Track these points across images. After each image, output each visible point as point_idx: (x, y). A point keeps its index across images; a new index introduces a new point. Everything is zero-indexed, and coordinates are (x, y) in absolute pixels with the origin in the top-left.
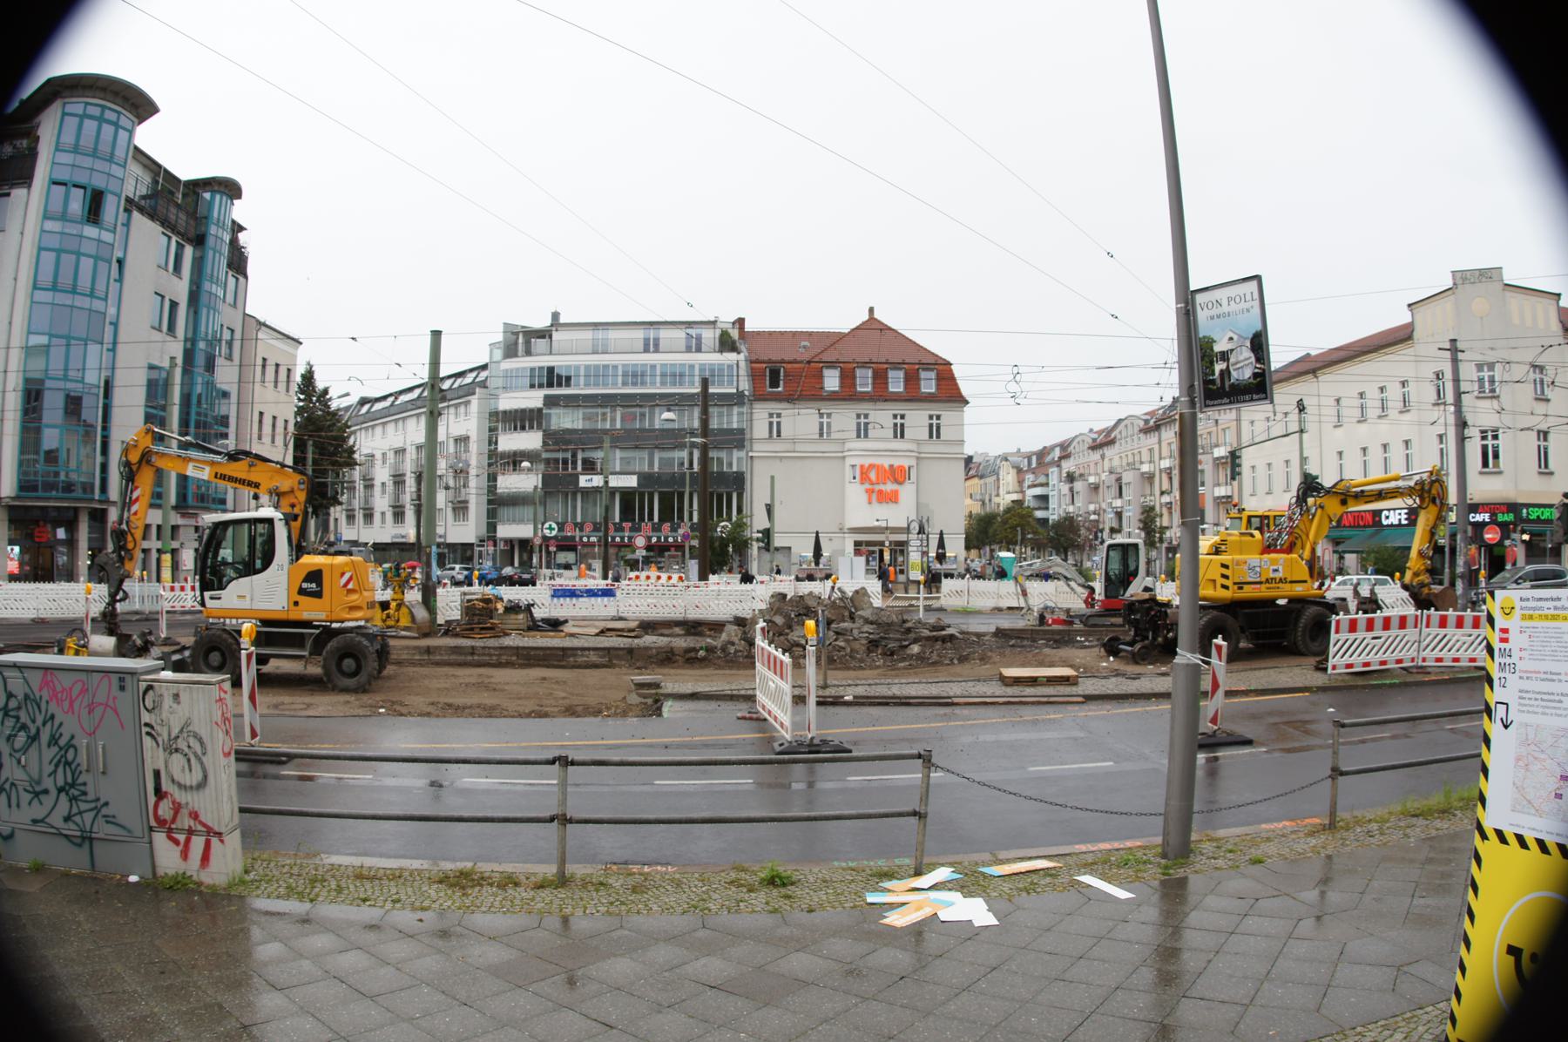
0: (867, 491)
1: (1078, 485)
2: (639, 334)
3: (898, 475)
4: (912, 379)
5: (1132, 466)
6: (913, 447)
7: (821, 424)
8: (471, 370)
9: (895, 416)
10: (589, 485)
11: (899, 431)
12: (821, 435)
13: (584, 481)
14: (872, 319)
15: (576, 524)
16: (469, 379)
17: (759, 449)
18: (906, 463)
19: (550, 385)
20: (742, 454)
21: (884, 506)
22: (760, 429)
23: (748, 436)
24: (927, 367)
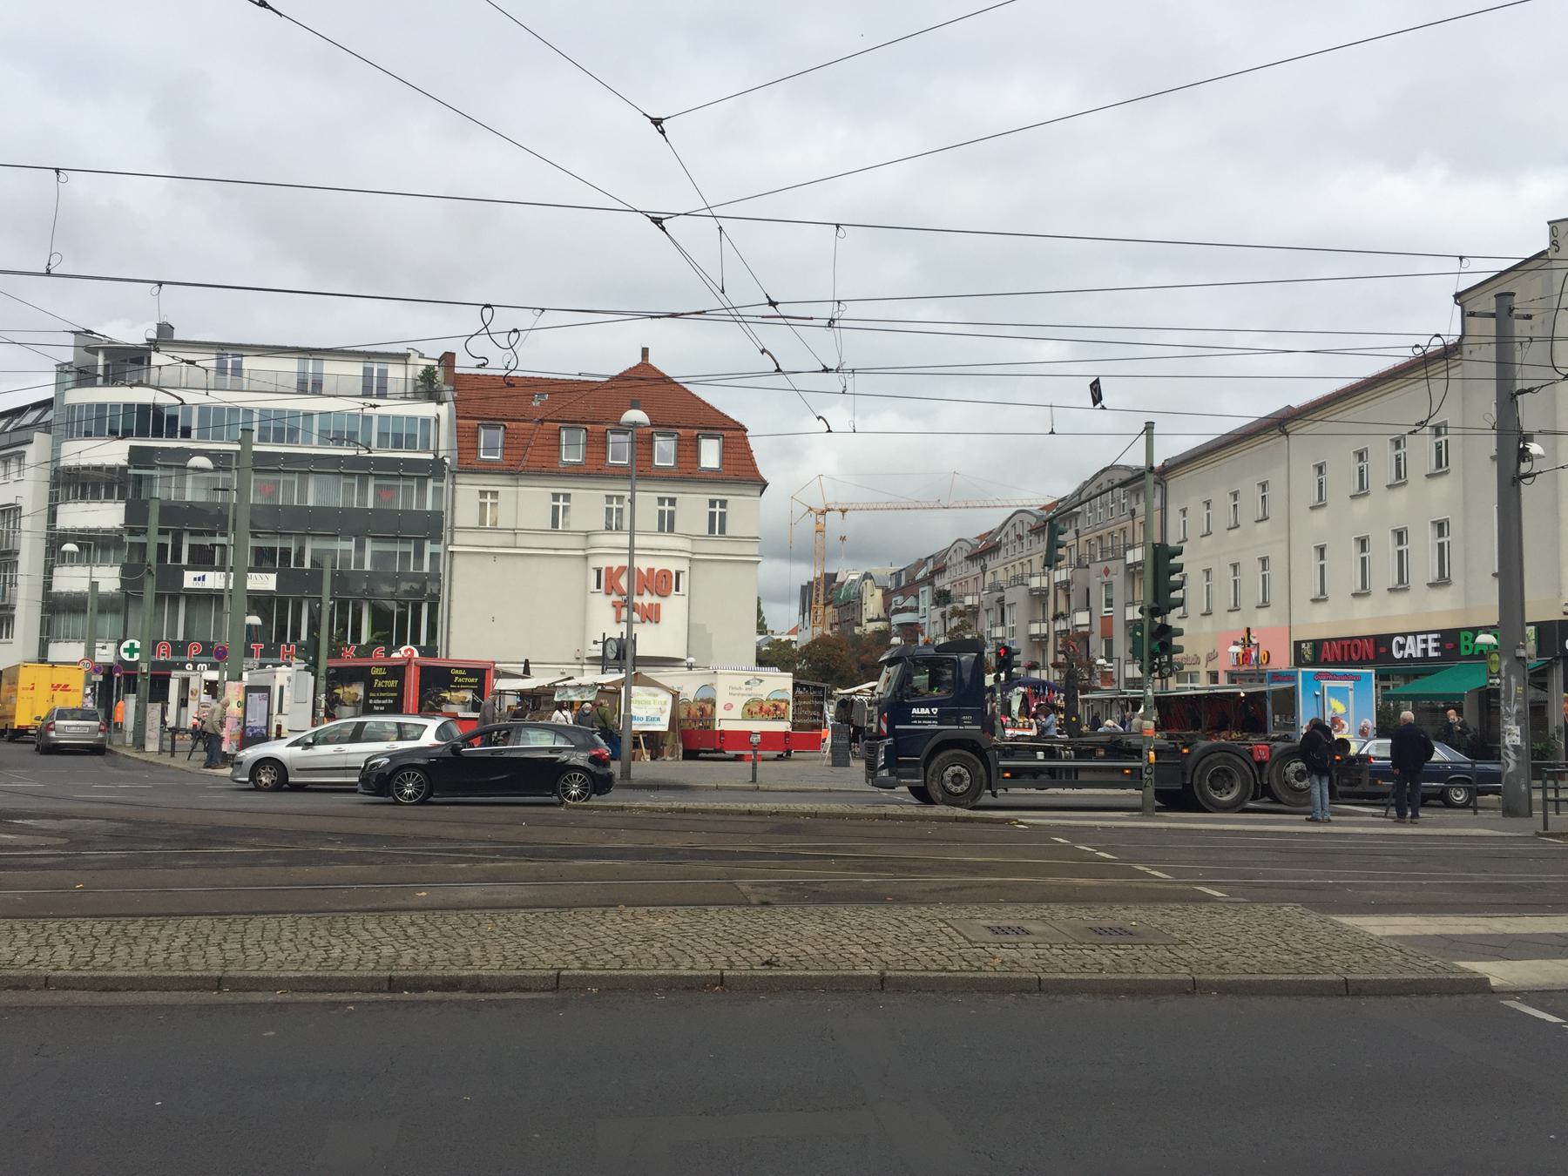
0: (614, 605)
2: (290, 365)
3: (663, 583)
4: (688, 450)
5: (1019, 581)
6: (684, 544)
7: (556, 509)
8: (35, 406)
9: (661, 501)
10: (199, 585)
11: (667, 524)
13: (190, 580)
14: (645, 364)
15: (174, 644)
16: (29, 418)
18: (673, 566)
19: (142, 433)
20: (439, 548)
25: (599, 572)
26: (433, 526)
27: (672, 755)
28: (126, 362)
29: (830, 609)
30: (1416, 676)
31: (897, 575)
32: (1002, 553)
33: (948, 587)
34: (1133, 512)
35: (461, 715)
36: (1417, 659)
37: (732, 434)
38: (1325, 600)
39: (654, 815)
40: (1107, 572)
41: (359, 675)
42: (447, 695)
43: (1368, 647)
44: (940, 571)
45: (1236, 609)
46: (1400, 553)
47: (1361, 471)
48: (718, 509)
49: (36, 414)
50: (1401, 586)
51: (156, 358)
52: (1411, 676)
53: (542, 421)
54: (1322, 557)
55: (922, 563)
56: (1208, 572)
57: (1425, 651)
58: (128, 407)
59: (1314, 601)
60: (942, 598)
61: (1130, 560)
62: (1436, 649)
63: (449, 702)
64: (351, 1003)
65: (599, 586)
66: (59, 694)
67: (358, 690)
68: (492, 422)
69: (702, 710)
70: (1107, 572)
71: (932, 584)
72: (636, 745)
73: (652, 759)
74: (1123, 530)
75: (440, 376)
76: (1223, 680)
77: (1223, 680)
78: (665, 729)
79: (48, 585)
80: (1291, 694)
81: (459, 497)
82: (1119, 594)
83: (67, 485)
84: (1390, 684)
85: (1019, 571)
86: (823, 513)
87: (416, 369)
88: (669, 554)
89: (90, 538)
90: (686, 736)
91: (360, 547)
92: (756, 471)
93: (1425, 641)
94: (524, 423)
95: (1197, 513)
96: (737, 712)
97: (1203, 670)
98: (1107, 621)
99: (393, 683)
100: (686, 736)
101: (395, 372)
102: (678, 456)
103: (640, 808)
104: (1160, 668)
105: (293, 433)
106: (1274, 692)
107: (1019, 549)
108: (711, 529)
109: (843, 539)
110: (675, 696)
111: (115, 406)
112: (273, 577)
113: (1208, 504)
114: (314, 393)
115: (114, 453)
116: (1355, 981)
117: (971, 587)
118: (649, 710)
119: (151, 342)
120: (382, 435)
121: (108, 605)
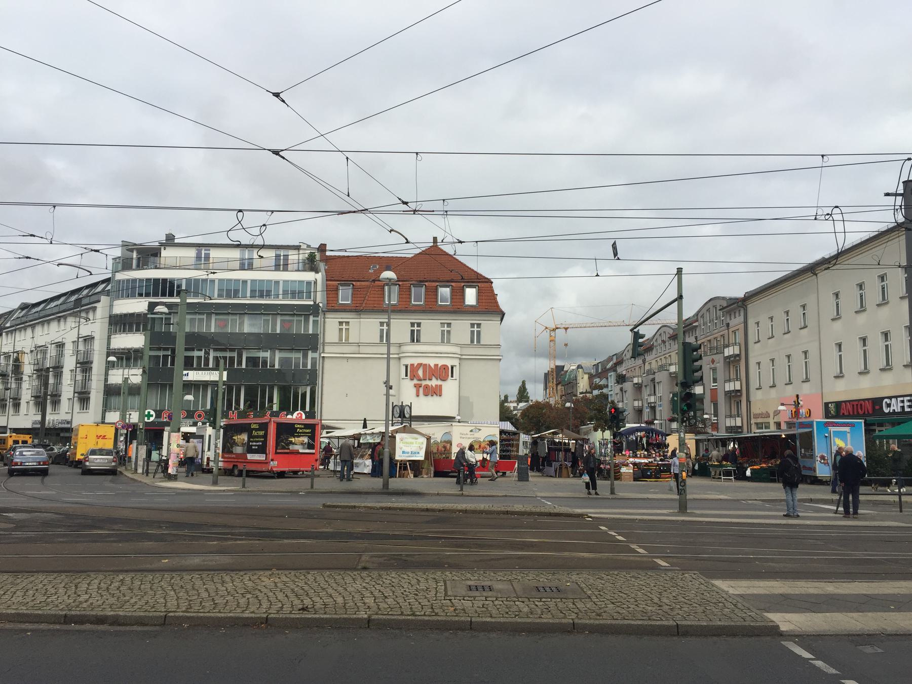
0: (415, 386)
1: (628, 386)
2: (236, 254)
3: (443, 373)
4: (459, 295)
5: (662, 368)
6: (457, 350)
7: (382, 331)
11: (445, 338)
12: (413, 341)
17: (329, 351)
18: (449, 363)
19: (156, 295)
20: (316, 355)
25: (407, 367)
26: (312, 343)
27: (427, 474)
28: (148, 255)
29: (559, 387)
30: (899, 424)
31: (596, 366)
32: (654, 351)
33: (624, 373)
34: (728, 325)
35: (301, 451)
36: (898, 413)
37: (483, 284)
38: (842, 377)
39: (372, 511)
40: (713, 361)
41: (245, 428)
42: (293, 440)
43: (869, 406)
44: (620, 363)
45: (790, 383)
46: (887, 346)
47: (861, 296)
48: (475, 329)
49: (103, 285)
50: (888, 368)
51: (165, 253)
52: (894, 424)
54: (840, 351)
55: (610, 359)
56: (773, 360)
57: (903, 407)
58: (148, 280)
59: (836, 377)
60: (621, 379)
61: (726, 354)
62: (909, 407)
63: (294, 444)
64: (31, 630)
66: (100, 441)
67: (244, 437)
68: (345, 282)
69: (445, 447)
70: (713, 361)
71: (615, 371)
72: (405, 469)
73: (415, 476)
74: (723, 336)
75: (318, 257)
76: (784, 426)
77: (784, 426)
78: (422, 458)
79: (106, 380)
80: (810, 436)
81: (327, 326)
82: (720, 375)
83: (116, 324)
84: (883, 428)
85: (664, 361)
86: (554, 330)
87: (304, 255)
88: (447, 356)
89: (122, 353)
90: (437, 463)
91: (305, 356)
92: (498, 306)
93: (903, 402)
94: (356, 281)
95: (765, 324)
97: (771, 421)
98: (714, 392)
99: (262, 433)
100: (437, 463)
101: (293, 256)
102: (452, 299)
103: (365, 507)
104: (689, 419)
105: (236, 292)
106: (801, 434)
107: (663, 349)
108: (472, 341)
109: (566, 345)
110: (429, 439)
111: (141, 280)
113: (771, 318)
114: (284, 270)
115: (139, 306)
116: (683, 626)
117: (637, 372)
118: (410, 447)
119: (162, 244)
120: (253, 291)
121: (134, 390)
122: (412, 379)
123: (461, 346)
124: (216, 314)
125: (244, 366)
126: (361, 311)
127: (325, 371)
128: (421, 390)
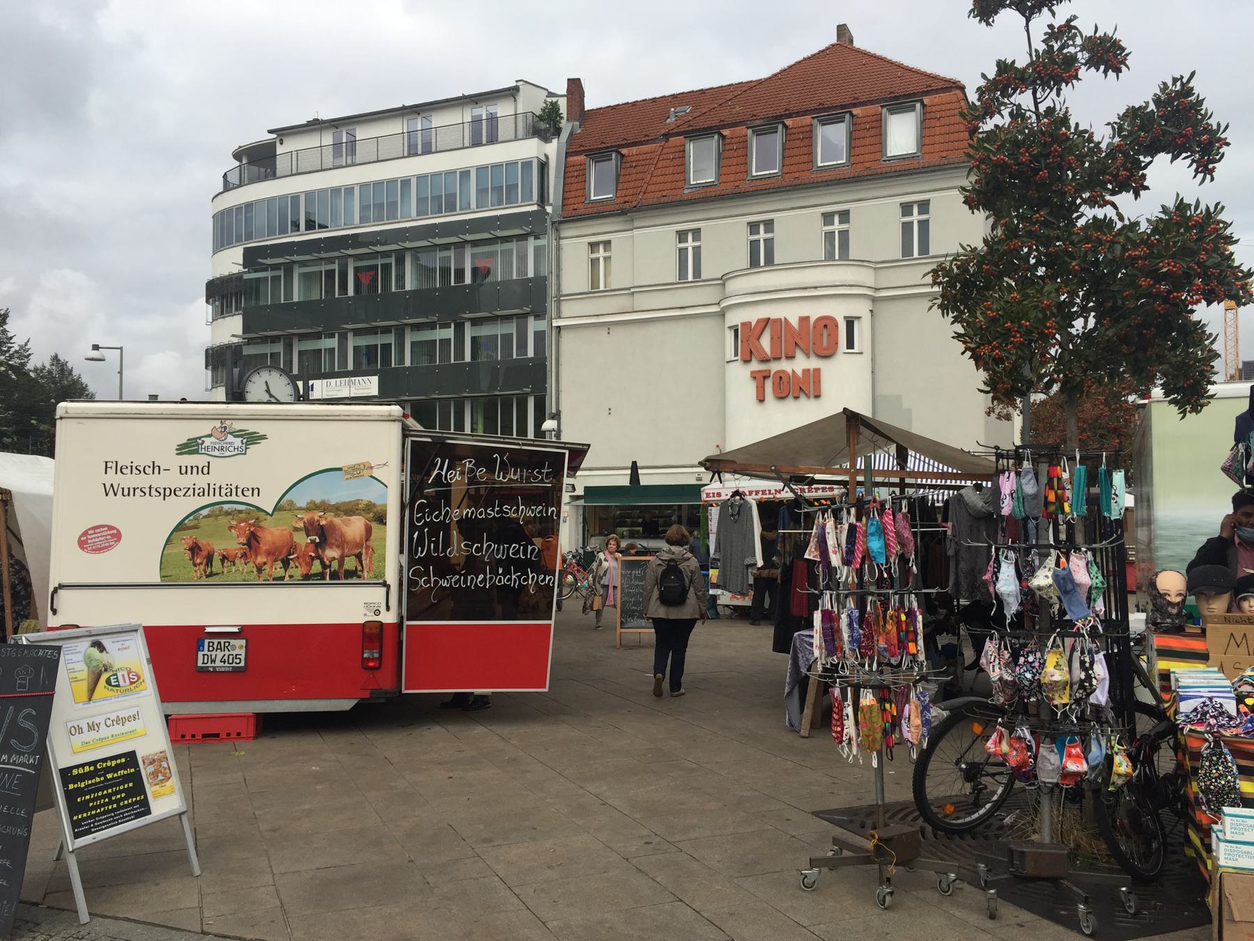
0: (754, 375)
3: (822, 338)
4: (868, 136)
6: (864, 276)
7: (682, 252)
11: (838, 248)
17: (571, 313)
18: (838, 311)
20: (542, 325)
21: (790, 403)
22: (574, 276)
23: (552, 291)
24: (899, 103)
26: (535, 297)
53: (667, 136)
65: (736, 355)
68: (599, 154)
96: (140, 555)
101: (503, 109)
102: (851, 147)
108: (907, 251)
112: (375, 380)
122: (747, 361)
123: (877, 266)
124: (475, 243)
125: (408, 363)
126: (629, 211)
127: (563, 360)
128: (769, 385)
